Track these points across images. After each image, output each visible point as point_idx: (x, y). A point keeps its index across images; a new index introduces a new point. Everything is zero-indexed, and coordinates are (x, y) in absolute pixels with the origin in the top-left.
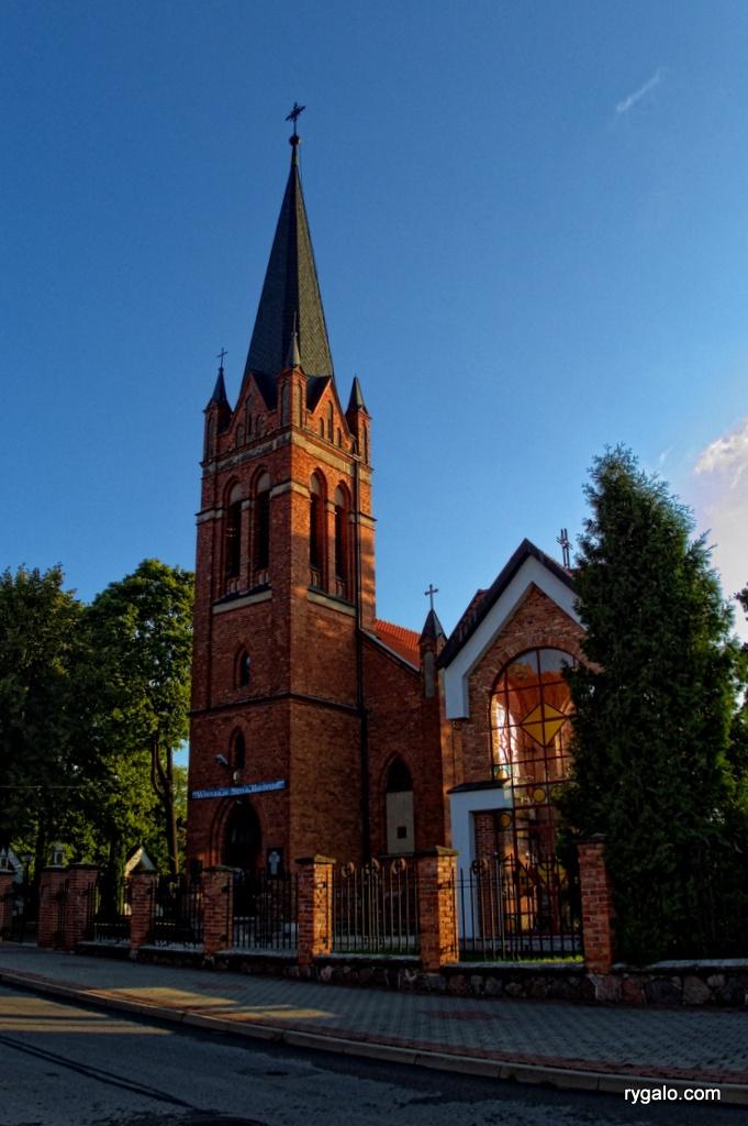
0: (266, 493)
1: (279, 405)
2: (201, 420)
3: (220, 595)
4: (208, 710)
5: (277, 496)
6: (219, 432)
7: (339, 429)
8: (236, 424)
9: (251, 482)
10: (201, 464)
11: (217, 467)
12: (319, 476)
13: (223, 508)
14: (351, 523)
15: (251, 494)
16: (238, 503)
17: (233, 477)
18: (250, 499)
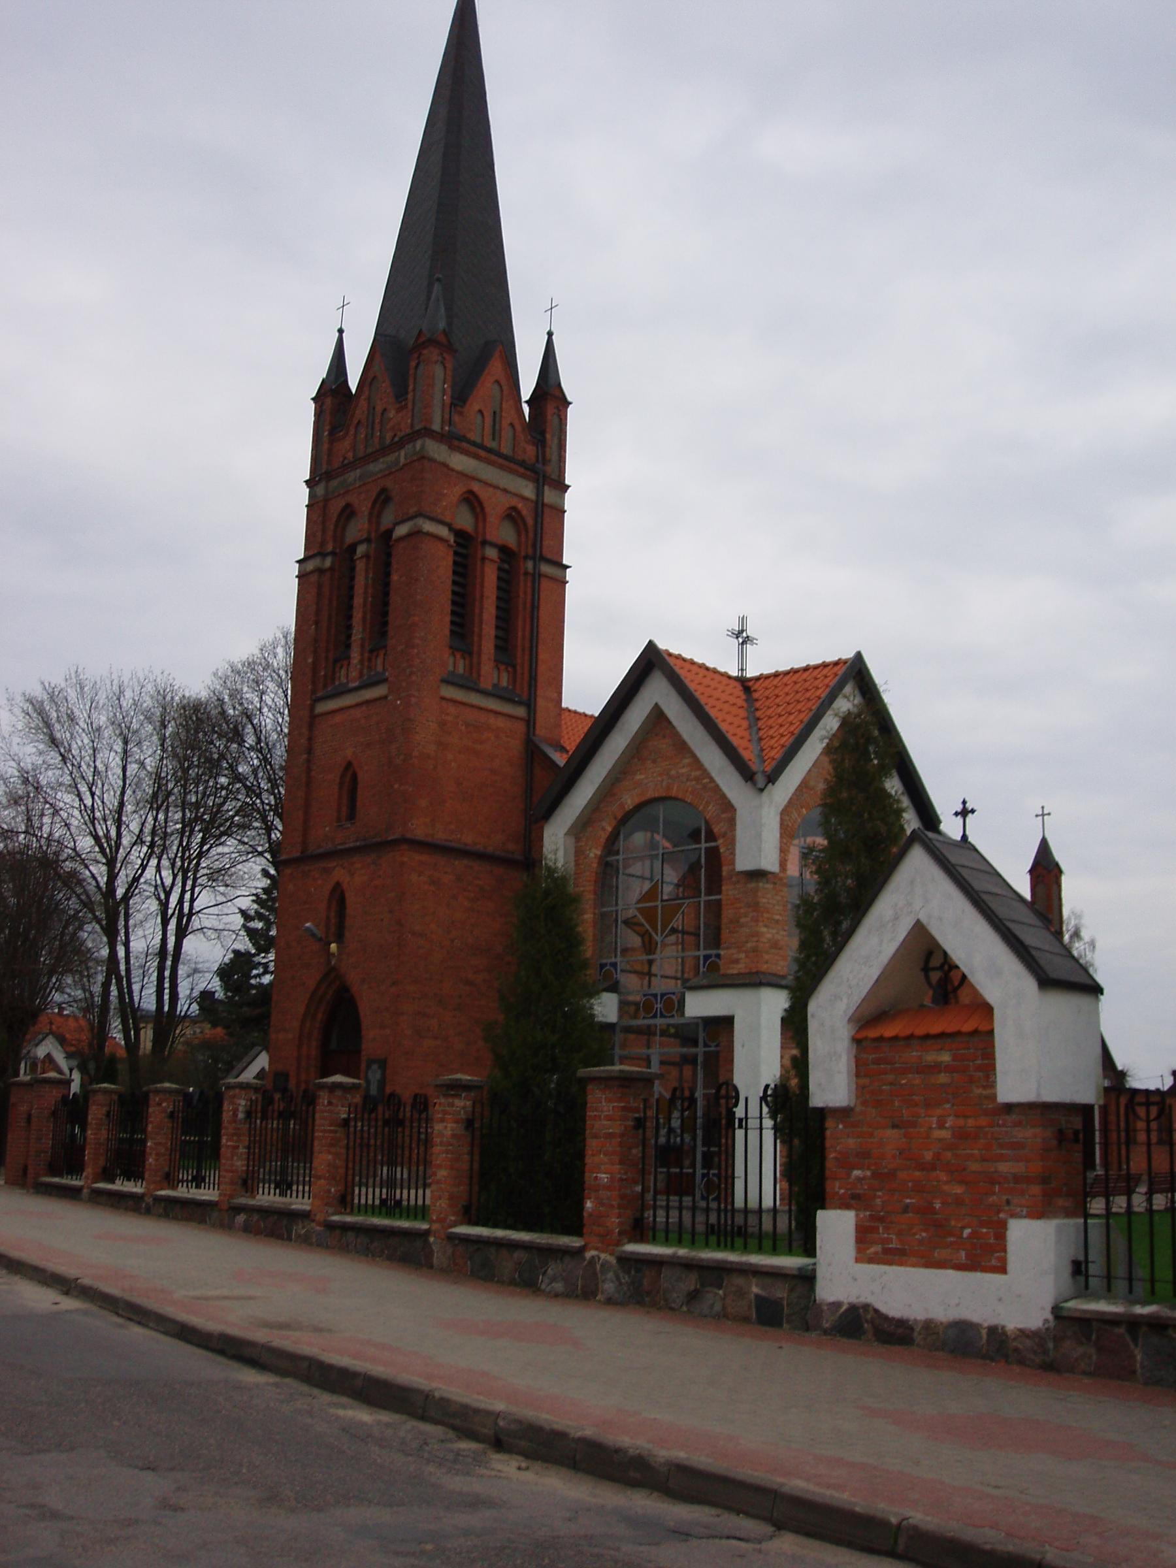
0: (389, 532)
1: (410, 396)
2: (309, 411)
3: (325, 686)
4: (306, 858)
5: (402, 539)
6: (331, 434)
7: (512, 425)
8: (355, 422)
9: (370, 514)
10: (306, 482)
11: (327, 488)
12: (472, 500)
13: (333, 553)
14: (526, 573)
15: (369, 532)
16: (353, 548)
17: (348, 505)
18: (368, 540)
